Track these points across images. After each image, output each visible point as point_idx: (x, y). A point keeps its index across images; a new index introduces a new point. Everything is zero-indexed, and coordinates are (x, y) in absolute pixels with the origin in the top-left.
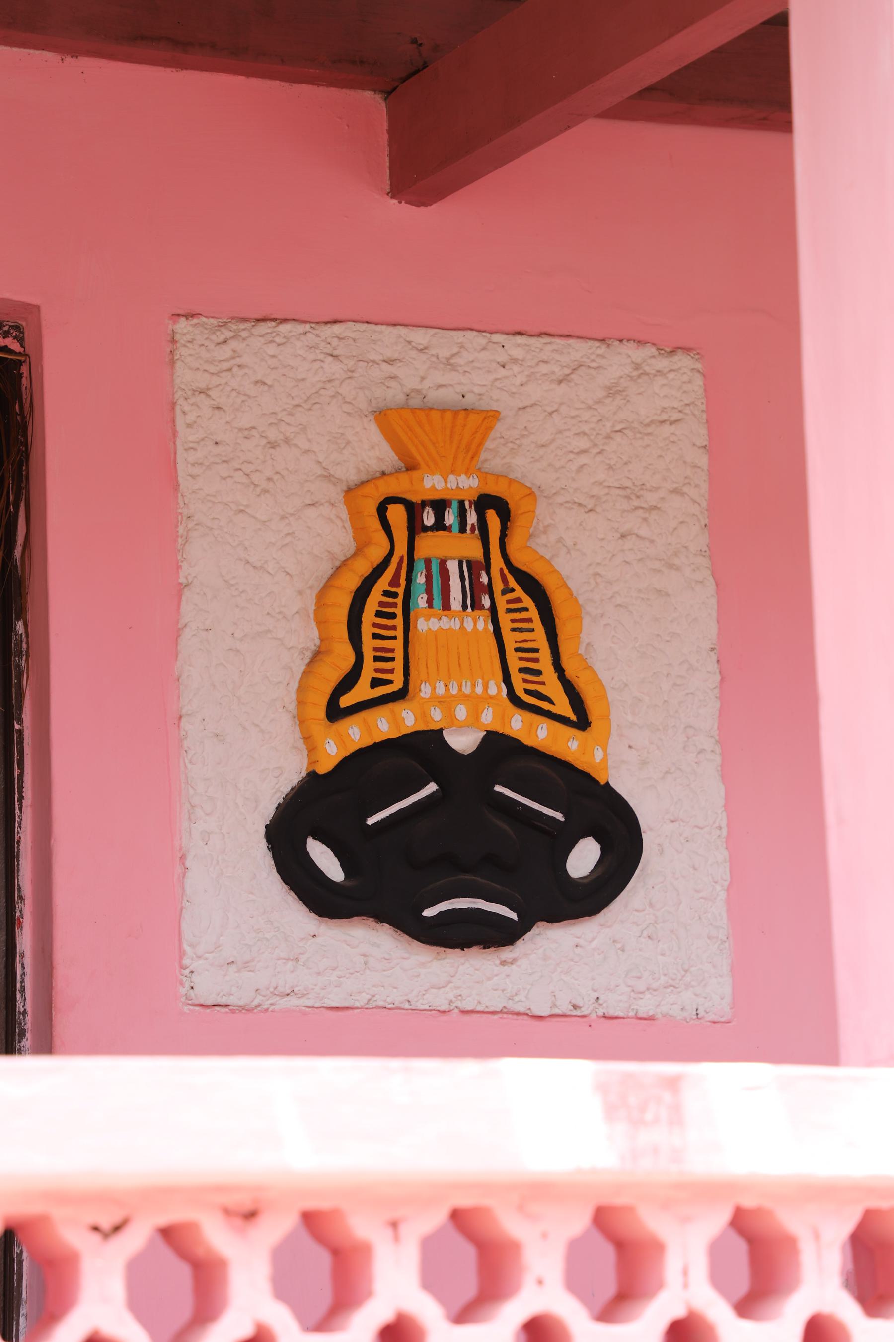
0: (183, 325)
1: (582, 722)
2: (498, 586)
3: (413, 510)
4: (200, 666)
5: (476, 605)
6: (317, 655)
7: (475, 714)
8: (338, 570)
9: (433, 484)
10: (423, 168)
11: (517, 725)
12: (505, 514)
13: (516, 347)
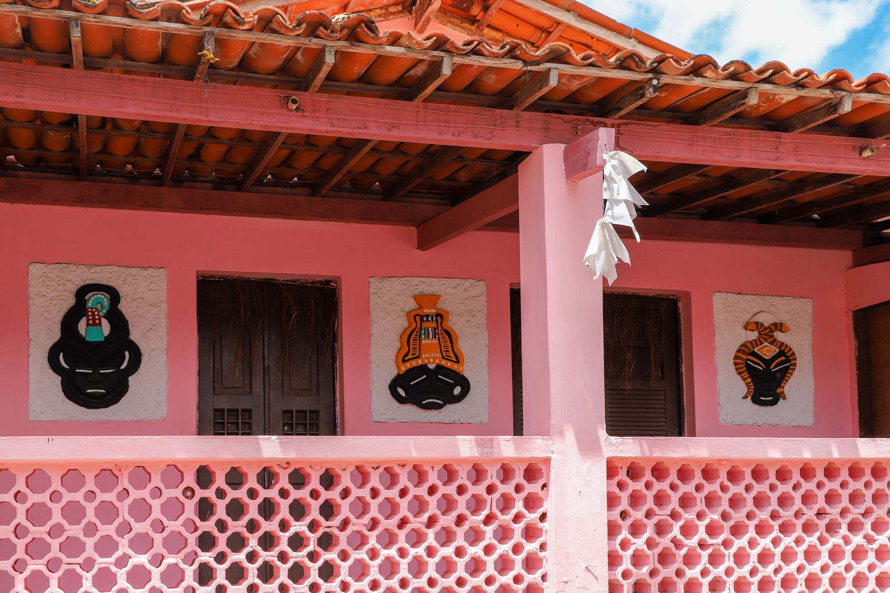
0: (372, 279)
1: (458, 362)
3: (422, 317)
4: (374, 352)
6: (400, 349)
7: (434, 361)
8: (405, 331)
9: (426, 311)
10: (424, 244)
11: (444, 362)
12: (442, 317)
13: (444, 281)
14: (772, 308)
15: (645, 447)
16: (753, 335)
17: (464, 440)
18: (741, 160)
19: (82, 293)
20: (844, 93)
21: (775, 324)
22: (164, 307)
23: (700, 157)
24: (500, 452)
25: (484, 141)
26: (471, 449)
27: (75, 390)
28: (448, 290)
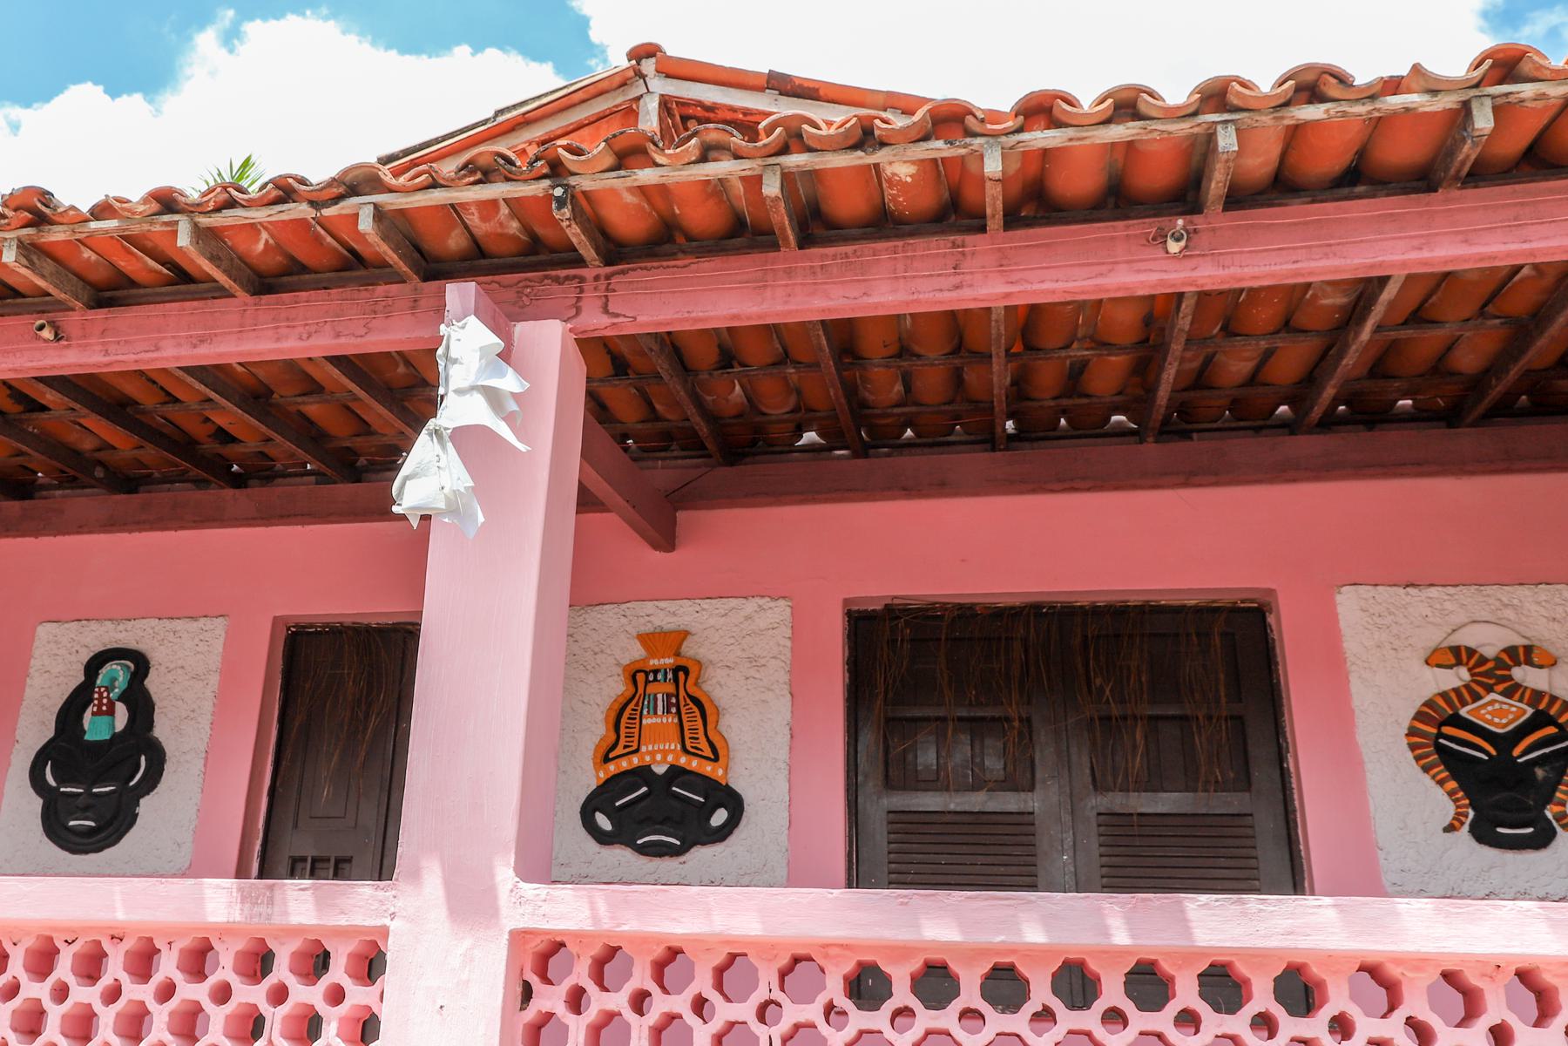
2: (682, 703)
5: (669, 712)
7: (664, 759)
9: (654, 662)
11: (683, 760)
12: (686, 671)
13: (705, 604)
14: (1509, 613)
15: (602, 907)
16: (1456, 678)
17: (218, 887)
18: (874, 299)
19: (95, 664)
20: (978, 141)
21: (1511, 651)
22: (214, 679)
23: (780, 308)
24: (286, 913)
25: (353, 340)
26: (230, 905)
27: (55, 826)
28: (712, 622)
